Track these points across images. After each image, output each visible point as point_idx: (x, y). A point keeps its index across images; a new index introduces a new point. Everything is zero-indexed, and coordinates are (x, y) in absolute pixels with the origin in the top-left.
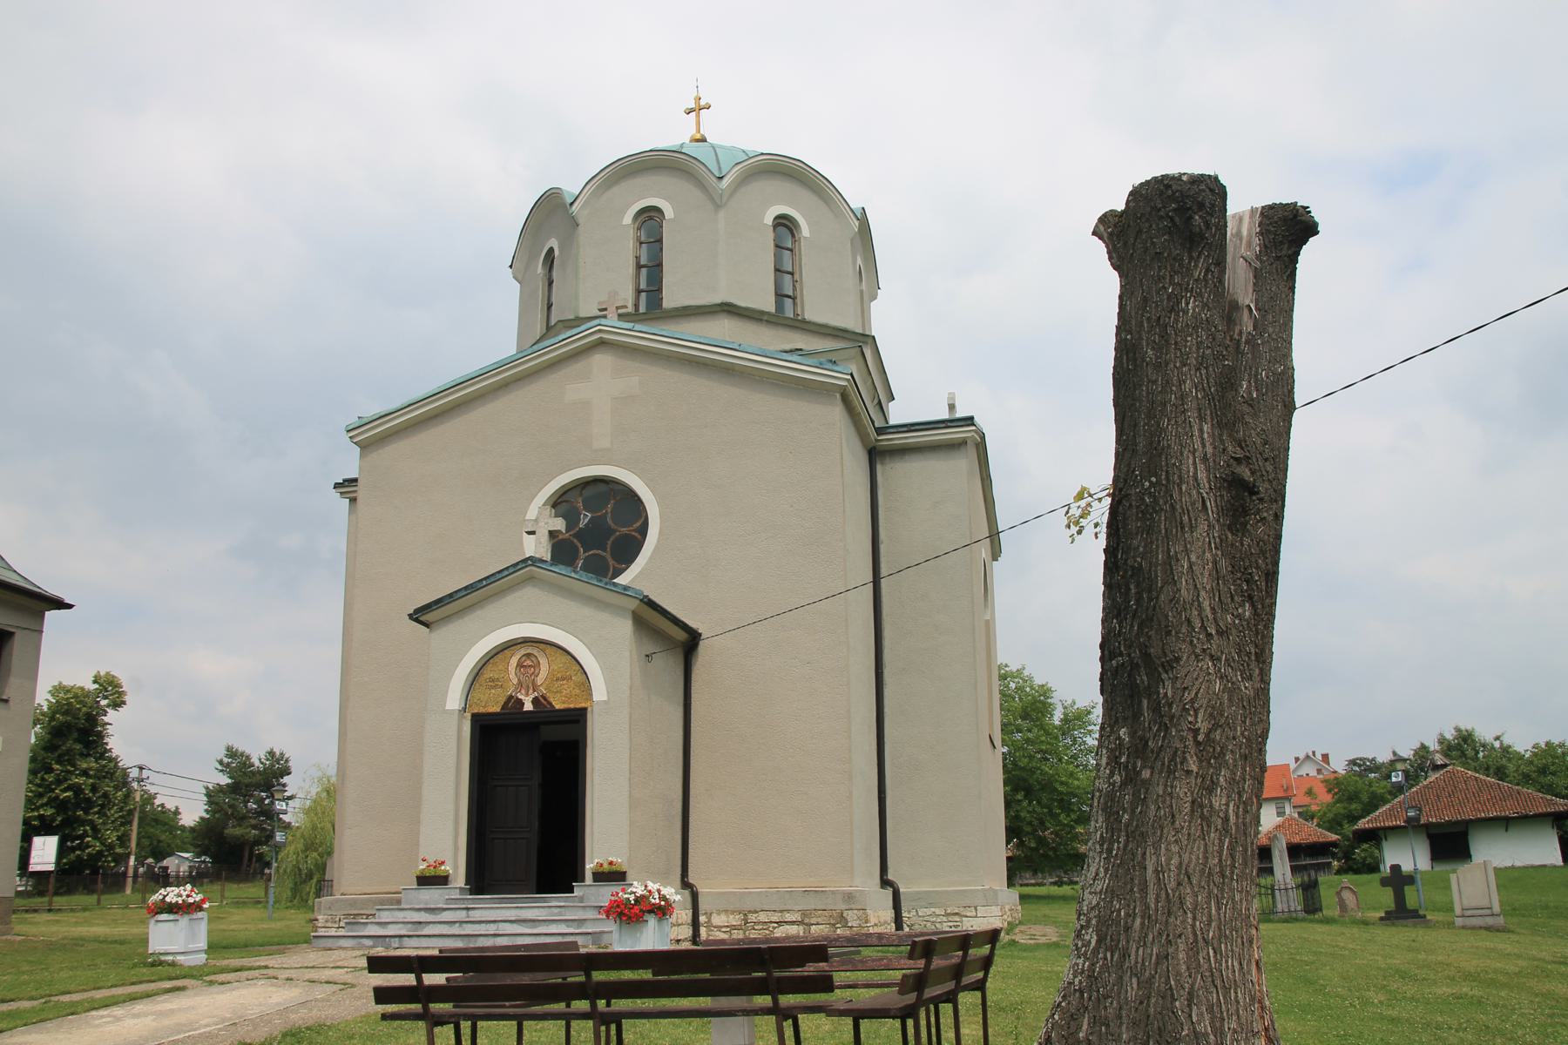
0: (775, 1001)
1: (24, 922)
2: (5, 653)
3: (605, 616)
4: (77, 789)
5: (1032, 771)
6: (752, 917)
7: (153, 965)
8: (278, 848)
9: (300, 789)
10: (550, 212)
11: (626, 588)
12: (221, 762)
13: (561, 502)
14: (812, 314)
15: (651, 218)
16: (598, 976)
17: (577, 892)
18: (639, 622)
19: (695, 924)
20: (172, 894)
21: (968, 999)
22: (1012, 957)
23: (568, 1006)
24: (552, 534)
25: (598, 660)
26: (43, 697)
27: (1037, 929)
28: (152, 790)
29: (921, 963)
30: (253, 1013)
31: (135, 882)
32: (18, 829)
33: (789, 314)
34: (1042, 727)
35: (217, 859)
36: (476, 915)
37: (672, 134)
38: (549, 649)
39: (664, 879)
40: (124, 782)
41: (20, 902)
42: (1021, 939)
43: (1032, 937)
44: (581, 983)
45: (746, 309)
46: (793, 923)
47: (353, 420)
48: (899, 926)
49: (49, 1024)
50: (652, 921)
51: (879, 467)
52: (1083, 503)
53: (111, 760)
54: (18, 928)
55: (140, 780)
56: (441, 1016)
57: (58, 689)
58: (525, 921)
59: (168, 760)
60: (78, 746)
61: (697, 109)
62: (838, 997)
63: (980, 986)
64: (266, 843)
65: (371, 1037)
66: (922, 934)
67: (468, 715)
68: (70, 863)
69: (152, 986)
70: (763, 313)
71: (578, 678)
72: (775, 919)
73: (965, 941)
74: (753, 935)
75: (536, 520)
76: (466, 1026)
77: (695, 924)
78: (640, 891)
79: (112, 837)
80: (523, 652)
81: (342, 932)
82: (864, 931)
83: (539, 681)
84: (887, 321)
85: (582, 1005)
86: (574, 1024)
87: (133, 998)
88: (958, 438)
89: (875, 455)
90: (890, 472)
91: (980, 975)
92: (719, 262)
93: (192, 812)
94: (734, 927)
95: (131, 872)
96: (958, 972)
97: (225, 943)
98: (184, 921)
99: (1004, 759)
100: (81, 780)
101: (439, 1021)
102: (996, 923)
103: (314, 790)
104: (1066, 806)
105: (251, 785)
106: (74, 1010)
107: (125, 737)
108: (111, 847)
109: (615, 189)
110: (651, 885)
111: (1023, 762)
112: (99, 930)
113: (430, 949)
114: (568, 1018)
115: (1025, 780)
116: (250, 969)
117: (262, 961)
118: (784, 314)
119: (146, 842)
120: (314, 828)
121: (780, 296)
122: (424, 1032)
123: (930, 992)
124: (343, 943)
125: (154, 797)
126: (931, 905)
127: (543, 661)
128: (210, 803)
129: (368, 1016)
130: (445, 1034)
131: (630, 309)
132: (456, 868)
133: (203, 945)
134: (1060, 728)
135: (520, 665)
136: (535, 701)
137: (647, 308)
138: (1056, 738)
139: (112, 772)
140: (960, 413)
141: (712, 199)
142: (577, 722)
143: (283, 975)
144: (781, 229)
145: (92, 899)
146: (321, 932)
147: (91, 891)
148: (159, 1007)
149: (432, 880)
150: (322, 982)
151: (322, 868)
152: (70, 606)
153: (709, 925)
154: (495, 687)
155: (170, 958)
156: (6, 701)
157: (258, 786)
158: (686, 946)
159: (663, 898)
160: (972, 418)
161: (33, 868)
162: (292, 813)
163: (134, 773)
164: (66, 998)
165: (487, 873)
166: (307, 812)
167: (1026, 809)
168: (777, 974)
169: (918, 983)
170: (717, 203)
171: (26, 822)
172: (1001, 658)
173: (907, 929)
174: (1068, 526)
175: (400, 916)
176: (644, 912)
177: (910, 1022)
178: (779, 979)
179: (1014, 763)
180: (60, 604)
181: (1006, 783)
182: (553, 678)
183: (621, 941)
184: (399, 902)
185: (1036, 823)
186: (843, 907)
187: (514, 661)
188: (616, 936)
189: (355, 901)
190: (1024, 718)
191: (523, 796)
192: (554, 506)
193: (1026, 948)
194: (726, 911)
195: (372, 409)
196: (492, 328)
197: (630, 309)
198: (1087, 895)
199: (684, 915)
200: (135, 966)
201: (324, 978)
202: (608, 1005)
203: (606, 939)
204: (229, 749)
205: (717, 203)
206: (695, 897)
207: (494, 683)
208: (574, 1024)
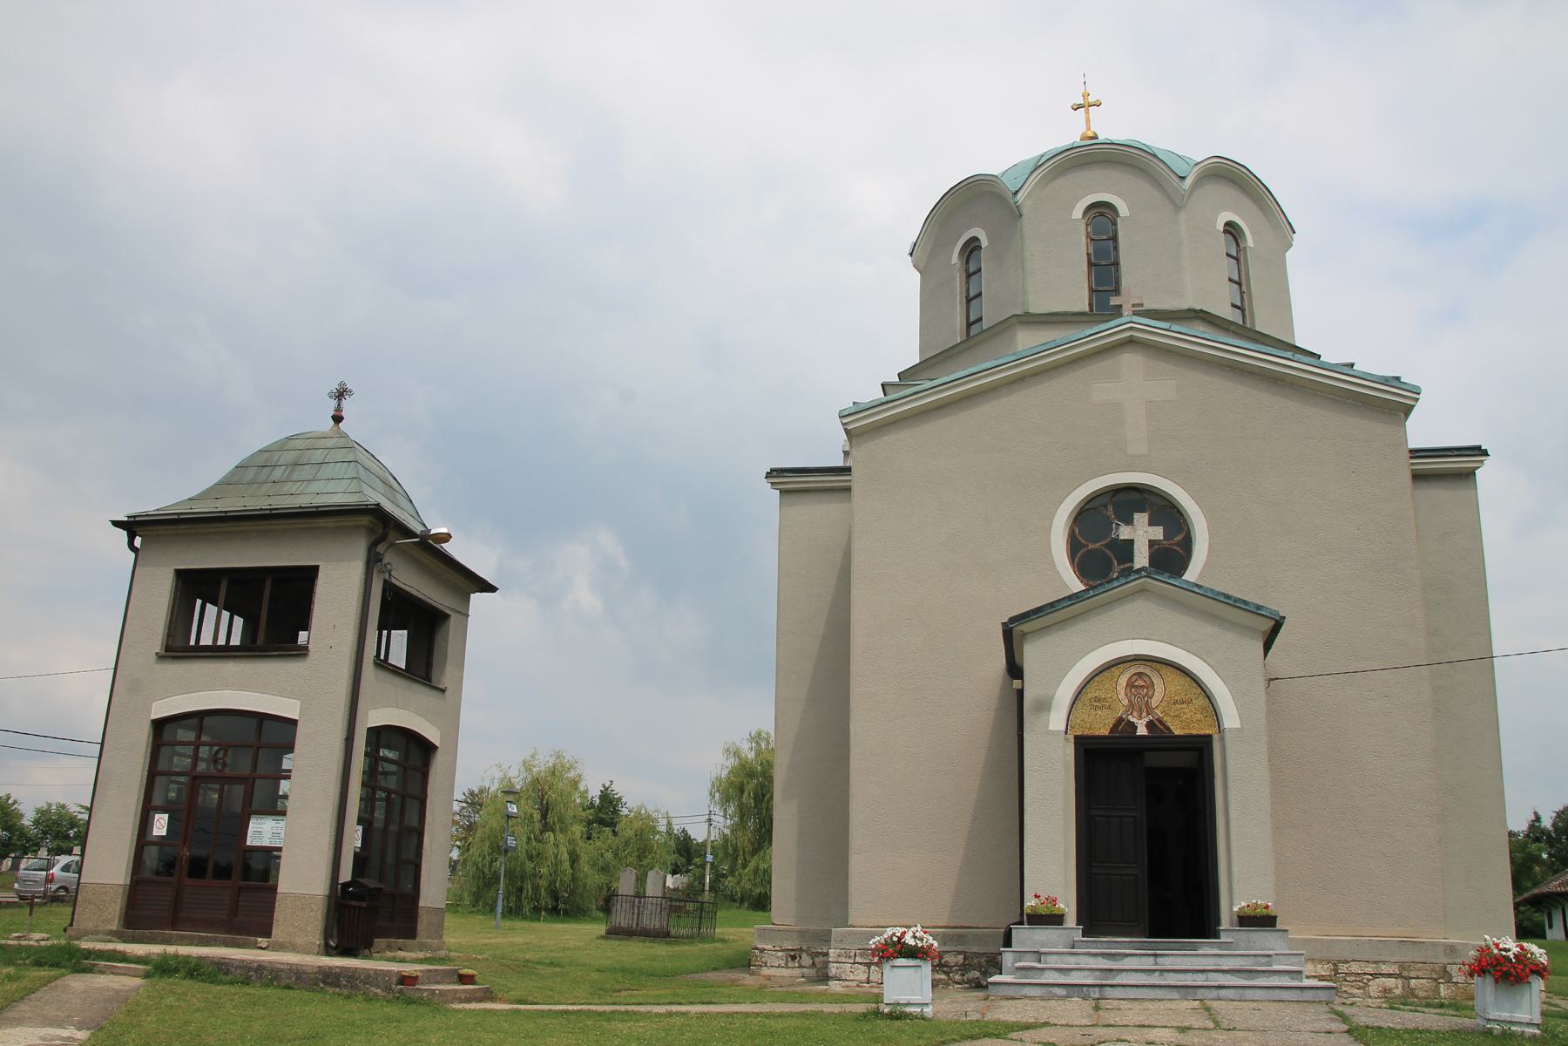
3: (1231, 636)
6: (1343, 968)
15: (1102, 214)
24: (1152, 543)
36: (1167, 963)
37: (1067, 133)
38: (1165, 670)
46: (1390, 975)
47: (847, 405)
71: (1201, 701)
72: (1369, 970)
80: (1133, 670)
92: (1173, 268)
109: (1061, 182)
127: (1157, 681)
135: (1130, 685)
136: (1150, 725)
141: (1172, 201)
156: (443, 691)
186: (1445, 961)
187: (1123, 681)
194: (1313, 960)
205: (1177, 203)
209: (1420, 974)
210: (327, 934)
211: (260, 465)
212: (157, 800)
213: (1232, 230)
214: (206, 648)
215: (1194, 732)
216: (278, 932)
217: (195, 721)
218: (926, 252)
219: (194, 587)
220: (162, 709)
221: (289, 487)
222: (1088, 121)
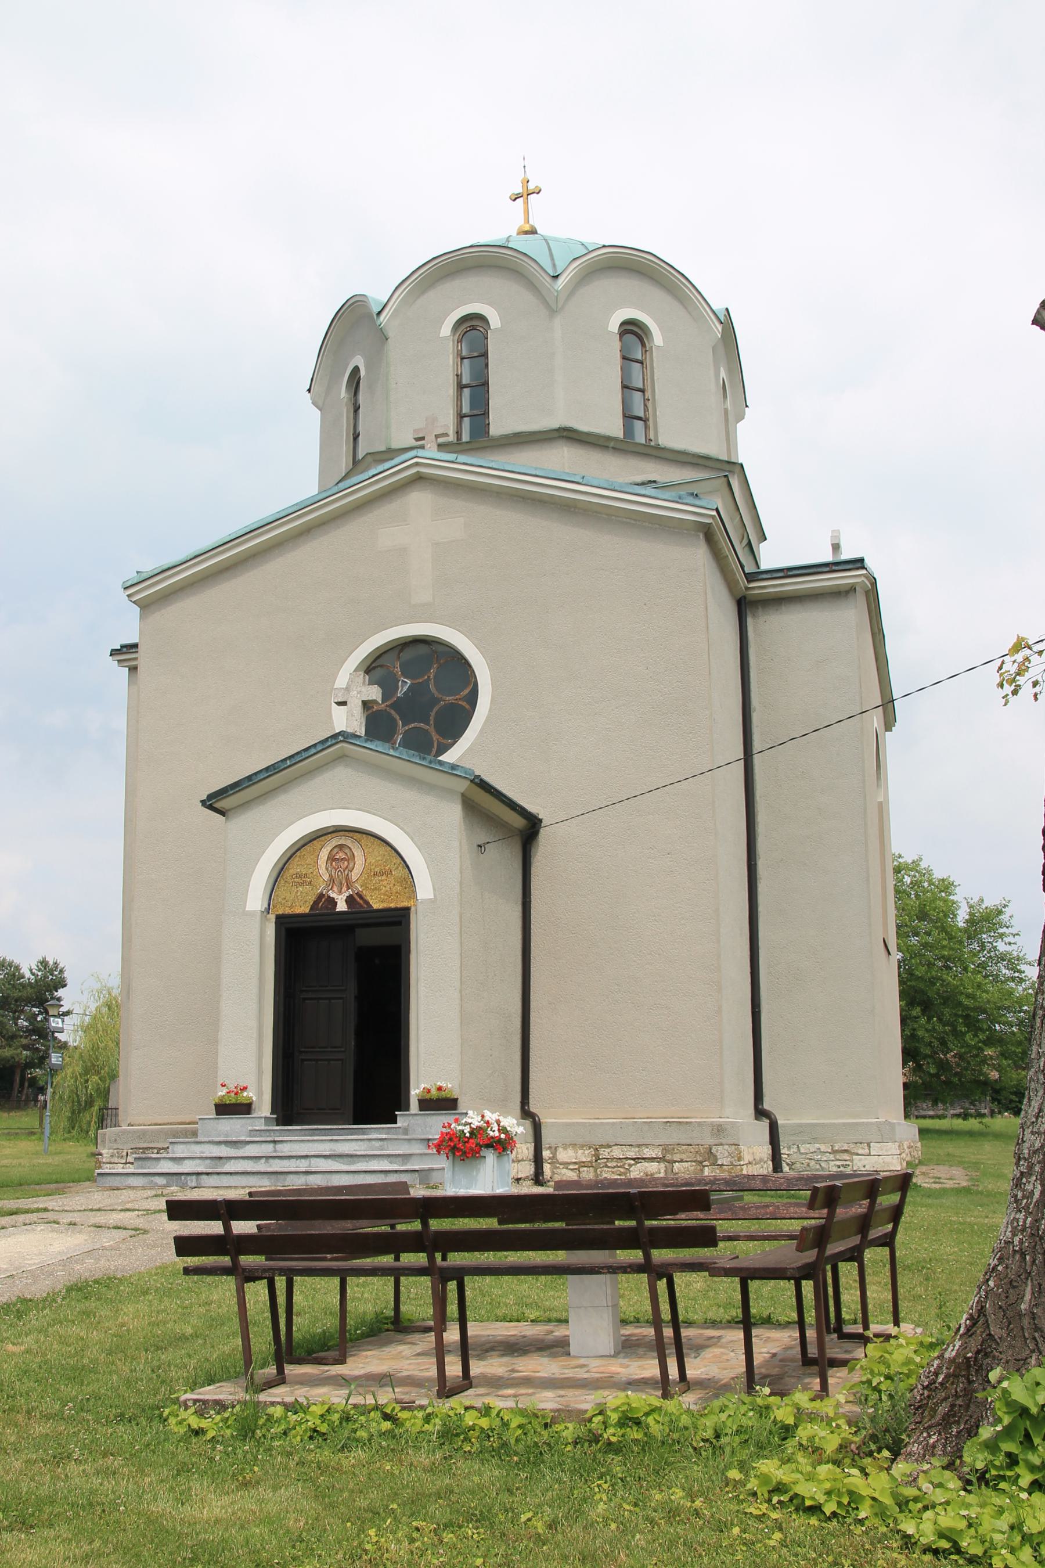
0: (647, 1256)
3: (428, 800)
5: (932, 982)
6: (605, 1153)
8: (54, 1071)
10: (354, 325)
11: (454, 767)
13: (375, 667)
14: (669, 437)
15: (473, 328)
16: (436, 1224)
17: (401, 1122)
18: (469, 806)
19: (538, 1160)
21: (874, 1255)
23: (397, 1259)
24: (365, 703)
27: (942, 1171)
30: (33, 1262)
34: (943, 929)
36: (285, 1149)
37: (495, 225)
39: (501, 1106)
43: (937, 1180)
45: (588, 434)
46: (652, 1159)
47: (131, 576)
48: (777, 1167)
50: (490, 1157)
51: (750, 621)
52: (1019, 657)
56: (252, 1270)
58: (340, 1156)
61: (525, 194)
63: (888, 1241)
65: (168, 1293)
66: (824, 1178)
67: (272, 917)
70: (608, 438)
72: (632, 1155)
73: (872, 1187)
74: (607, 1174)
75: (347, 689)
76: (281, 1283)
77: (538, 1160)
78: (476, 1122)
80: (335, 842)
81: (131, 1169)
82: (736, 1171)
83: (354, 876)
84: (754, 446)
85: (420, 1259)
88: (844, 585)
90: (764, 627)
92: (550, 379)
94: (583, 1164)
99: (899, 967)
101: (249, 1276)
103: (93, 1007)
104: (972, 1024)
109: (431, 294)
114: (397, 1273)
115: (923, 992)
116: (27, 1211)
117: (41, 1203)
118: (634, 438)
120: (95, 1048)
121: (628, 418)
123: (834, 1248)
126: (815, 1140)
127: (358, 853)
129: (164, 1267)
130: (257, 1292)
131: (452, 438)
132: (260, 1094)
134: (966, 931)
135: (331, 858)
136: (350, 900)
137: (471, 437)
138: (961, 942)
140: (846, 555)
142: (399, 923)
143: (66, 1218)
149: (233, 1108)
151: (105, 1094)
153: (554, 1160)
154: (302, 884)
157: (29, 1001)
159: (503, 1130)
160: (862, 560)
162: (68, 1030)
165: (293, 1104)
168: (649, 1223)
169: (820, 1237)
170: (552, 308)
172: (896, 848)
173: (786, 1168)
174: (1001, 685)
175: (197, 1150)
176: (480, 1147)
177: (808, 1286)
178: (653, 1230)
181: (903, 994)
182: (374, 873)
183: (458, 1183)
184: (195, 1133)
186: (712, 1141)
187: (324, 854)
188: (448, 1174)
189: (144, 1133)
190: (920, 919)
191: (338, 1010)
192: (367, 671)
194: (574, 1145)
195: (149, 566)
196: (287, 463)
198: (1028, 1136)
199: (525, 1149)
202: (444, 1258)
203: (435, 1178)
205: (552, 308)
207: (302, 879)
209: (684, 1157)
213: (632, 330)
215: (392, 905)
222: (527, 212)
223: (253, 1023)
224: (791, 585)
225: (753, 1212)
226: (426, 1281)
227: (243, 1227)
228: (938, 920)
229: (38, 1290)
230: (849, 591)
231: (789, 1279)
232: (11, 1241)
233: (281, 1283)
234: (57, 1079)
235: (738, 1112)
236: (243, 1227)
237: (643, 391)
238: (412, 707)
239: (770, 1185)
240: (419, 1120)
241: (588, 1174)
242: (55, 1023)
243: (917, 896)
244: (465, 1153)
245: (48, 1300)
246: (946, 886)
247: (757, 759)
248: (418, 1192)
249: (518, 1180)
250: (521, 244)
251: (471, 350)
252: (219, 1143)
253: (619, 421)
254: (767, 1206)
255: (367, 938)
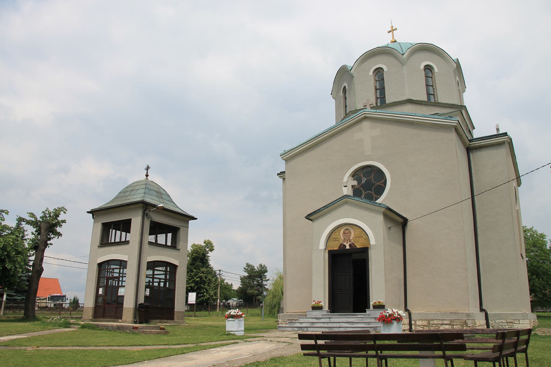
0: (444, 353)
1: (187, 319)
2: (178, 234)
3: (373, 214)
4: (201, 278)
5: (539, 267)
6: (431, 322)
7: (228, 335)
8: (265, 297)
9: (271, 277)
10: (344, 74)
11: (380, 204)
12: (245, 268)
13: (355, 175)
14: (441, 99)
15: (379, 72)
16: (378, 342)
17: (367, 312)
18: (385, 216)
19: (410, 324)
20: (233, 312)
22: (536, 340)
23: (367, 353)
24: (352, 186)
25: (371, 229)
26: (189, 249)
27: (545, 330)
28: (224, 278)
29: (500, 341)
30: (260, 351)
31: (220, 307)
32: (185, 290)
33: (433, 101)
34: (542, 250)
35: (244, 301)
36: (332, 320)
37: (384, 41)
39: (398, 307)
40: (215, 275)
41: (186, 313)
42: (539, 333)
43: (544, 332)
44: (372, 345)
45: (416, 101)
47: (282, 152)
49: (198, 352)
50: (395, 323)
51: (471, 155)
53: (211, 268)
54: (187, 321)
55: (220, 275)
57: (194, 246)
59: (229, 268)
60: (200, 264)
61: (392, 31)
62: (468, 352)
63: (525, 351)
64: (260, 295)
65: (299, 361)
66: (501, 330)
67: (327, 251)
68: (200, 301)
69: (228, 342)
70: (423, 101)
71: (365, 237)
72: (440, 323)
73: (518, 333)
74: (432, 329)
75: (347, 182)
76: (332, 359)
77: (410, 324)
78: (390, 312)
79: (212, 293)
81: (287, 325)
85: (373, 353)
86: (369, 359)
87: (222, 345)
88: (502, 141)
89: (469, 150)
90: (476, 156)
91: (525, 346)
92: (406, 85)
93: (236, 285)
94: (425, 326)
95: (218, 305)
96: (515, 345)
97: (249, 328)
98: (237, 320)
99: (527, 263)
100: (202, 275)
101: (323, 356)
102: (528, 327)
103: (275, 277)
105: (255, 276)
106: (205, 348)
107: (215, 260)
108: (212, 296)
109: (366, 63)
110: (394, 310)
111: (535, 264)
112: (210, 323)
113: (319, 332)
114: (367, 357)
116: (258, 337)
117: (262, 335)
118: (431, 101)
119: (222, 295)
120: (276, 290)
121: (429, 95)
122: (318, 360)
123: (505, 352)
124: (288, 329)
125: (224, 280)
126: (501, 319)
128: (242, 282)
129: (297, 354)
130: (325, 361)
131: (375, 105)
132: (325, 304)
133: (243, 329)
135: (344, 233)
136: (350, 245)
138: (548, 254)
139: (211, 272)
140: (501, 132)
142: (365, 252)
143: (269, 339)
144: (427, 70)
145: (207, 313)
146: (280, 325)
147: (207, 310)
148: (231, 348)
150: (281, 342)
151: (279, 304)
152: (196, 219)
153: (415, 324)
154: (336, 241)
155: (233, 333)
157: (257, 276)
158: (407, 332)
160: (506, 133)
161: (189, 303)
162: (269, 285)
163: (218, 272)
164: (202, 344)
165: (336, 306)
166: (274, 285)
167: (537, 282)
169: (500, 348)
171: (187, 288)
172: (524, 224)
173: (491, 328)
175: (306, 320)
176: (392, 320)
178: (445, 345)
179: (531, 265)
180: (193, 218)
181: (528, 272)
182: (356, 237)
183: (384, 330)
184: (306, 315)
185: (542, 287)
187: (342, 232)
188: (382, 328)
189: (291, 315)
192: (353, 176)
193: (541, 337)
194: (422, 320)
195: (288, 148)
196: (326, 116)
197: (375, 105)
199: (406, 321)
200: (222, 335)
201: (282, 341)
202: (381, 353)
203: (378, 329)
204: (247, 264)
206: (410, 314)
207: (335, 239)
208: (352, 358)
210: (135, 317)
211: (124, 192)
212: (101, 284)
213: (428, 68)
214: (113, 243)
216: (124, 318)
217: (107, 263)
218: (334, 93)
219: (107, 228)
220: (100, 260)
221: (129, 197)
222: (393, 36)
223: (322, 283)
224: (483, 142)
225: (479, 341)
226: (375, 359)
227: (320, 342)
228: (540, 247)
229: (262, 359)
230: (502, 143)
231: (490, 361)
232: (254, 345)
233: (332, 359)
234: (265, 299)
235: (475, 309)
236: (320, 342)
237: (432, 86)
238: (367, 186)
239: (484, 332)
240: (373, 312)
241: (426, 328)
242: (265, 283)
243: (532, 239)
244: (387, 322)
245: (265, 362)
246: (542, 236)
247: (476, 198)
248: (373, 333)
249: (404, 330)
250: (392, 45)
251: (379, 78)
252: (313, 318)
253: (426, 96)
254: (483, 339)
255: (355, 257)
